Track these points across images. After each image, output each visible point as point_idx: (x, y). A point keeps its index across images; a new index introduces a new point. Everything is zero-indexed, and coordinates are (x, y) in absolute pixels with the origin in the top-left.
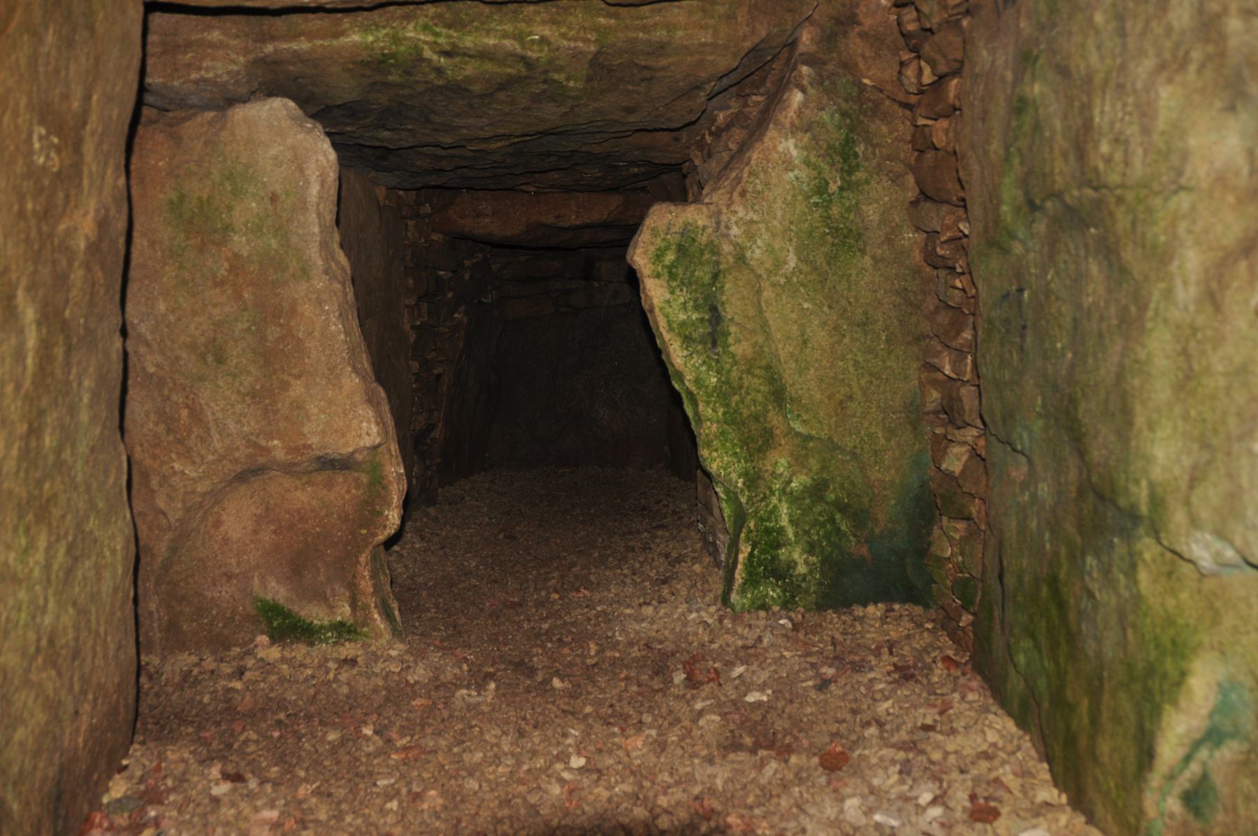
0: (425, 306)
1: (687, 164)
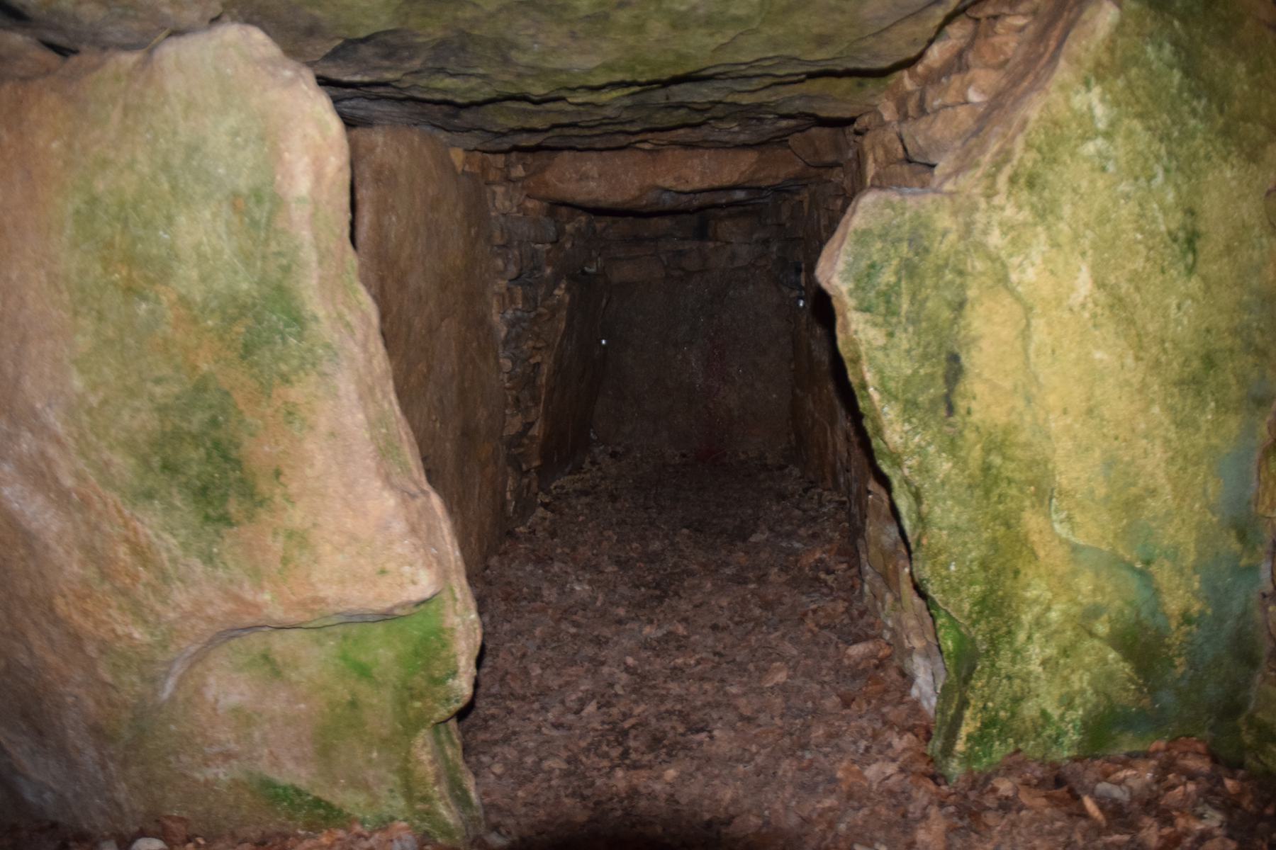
0: (519, 292)
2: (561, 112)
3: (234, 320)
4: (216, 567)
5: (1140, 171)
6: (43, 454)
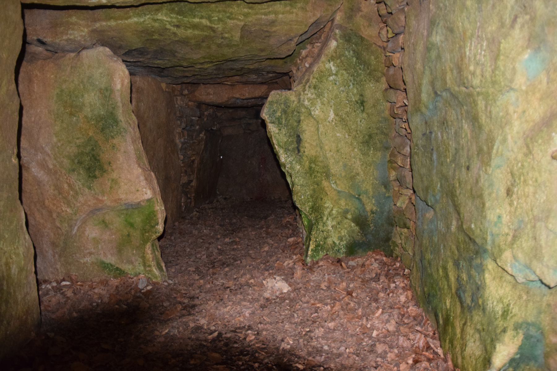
0: (186, 133)
1: (291, 73)
2: (194, 71)
3: (99, 122)
4: (92, 190)
5: (346, 84)
6: (44, 159)
